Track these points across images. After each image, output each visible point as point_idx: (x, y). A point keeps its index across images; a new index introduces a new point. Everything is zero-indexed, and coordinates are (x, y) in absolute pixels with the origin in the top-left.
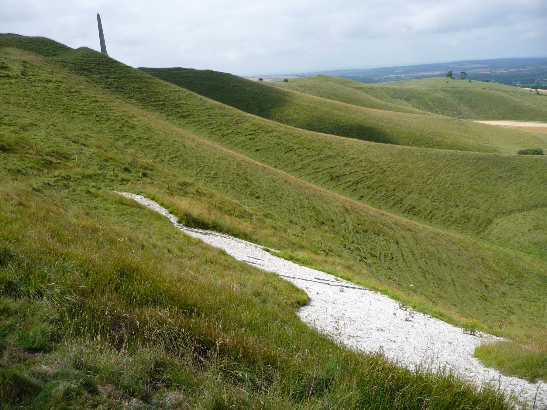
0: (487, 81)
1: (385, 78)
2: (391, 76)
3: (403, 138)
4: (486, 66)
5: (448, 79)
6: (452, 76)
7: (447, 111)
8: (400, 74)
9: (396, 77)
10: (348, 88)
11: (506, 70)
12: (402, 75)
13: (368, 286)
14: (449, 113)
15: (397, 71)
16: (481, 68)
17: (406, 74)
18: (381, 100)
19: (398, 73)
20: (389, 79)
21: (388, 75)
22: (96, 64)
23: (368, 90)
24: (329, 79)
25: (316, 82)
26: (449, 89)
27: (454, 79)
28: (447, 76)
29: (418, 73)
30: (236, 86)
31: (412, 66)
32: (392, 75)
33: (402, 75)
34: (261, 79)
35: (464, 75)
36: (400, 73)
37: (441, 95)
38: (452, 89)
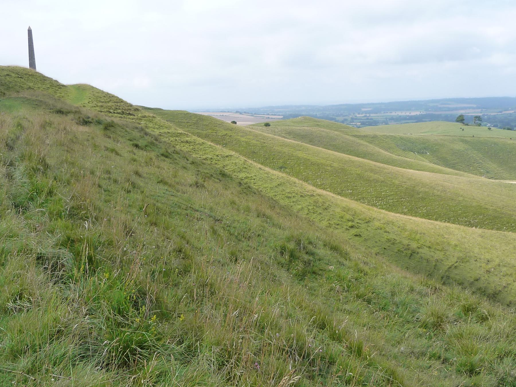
0: (508, 129)
1: (352, 119)
2: (358, 115)
3: (474, 214)
4: (475, 106)
5: (460, 125)
6: (464, 121)
7: (471, 168)
8: (369, 113)
9: (365, 116)
10: (348, 137)
11: (501, 112)
12: (371, 115)
13: (136, 306)
14: (474, 170)
15: (363, 110)
16: (470, 108)
17: (377, 114)
18: (391, 153)
19: (366, 112)
20: (356, 119)
21: (354, 114)
22: (119, 113)
23: (373, 139)
24: (319, 124)
25: (306, 128)
26: (468, 139)
27: (467, 125)
28: (457, 121)
29: (391, 113)
30: (226, 135)
31: (382, 104)
32: (359, 114)
33: (371, 115)
34: (234, 123)
35: (478, 120)
36: (370, 112)
37: (460, 147)
38: (472, 138)
